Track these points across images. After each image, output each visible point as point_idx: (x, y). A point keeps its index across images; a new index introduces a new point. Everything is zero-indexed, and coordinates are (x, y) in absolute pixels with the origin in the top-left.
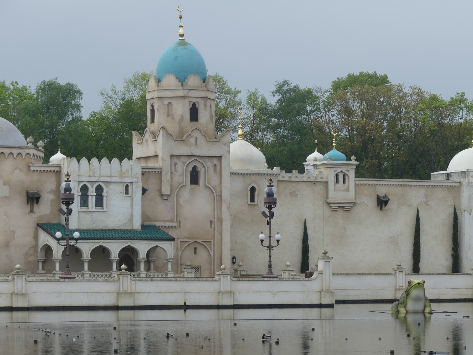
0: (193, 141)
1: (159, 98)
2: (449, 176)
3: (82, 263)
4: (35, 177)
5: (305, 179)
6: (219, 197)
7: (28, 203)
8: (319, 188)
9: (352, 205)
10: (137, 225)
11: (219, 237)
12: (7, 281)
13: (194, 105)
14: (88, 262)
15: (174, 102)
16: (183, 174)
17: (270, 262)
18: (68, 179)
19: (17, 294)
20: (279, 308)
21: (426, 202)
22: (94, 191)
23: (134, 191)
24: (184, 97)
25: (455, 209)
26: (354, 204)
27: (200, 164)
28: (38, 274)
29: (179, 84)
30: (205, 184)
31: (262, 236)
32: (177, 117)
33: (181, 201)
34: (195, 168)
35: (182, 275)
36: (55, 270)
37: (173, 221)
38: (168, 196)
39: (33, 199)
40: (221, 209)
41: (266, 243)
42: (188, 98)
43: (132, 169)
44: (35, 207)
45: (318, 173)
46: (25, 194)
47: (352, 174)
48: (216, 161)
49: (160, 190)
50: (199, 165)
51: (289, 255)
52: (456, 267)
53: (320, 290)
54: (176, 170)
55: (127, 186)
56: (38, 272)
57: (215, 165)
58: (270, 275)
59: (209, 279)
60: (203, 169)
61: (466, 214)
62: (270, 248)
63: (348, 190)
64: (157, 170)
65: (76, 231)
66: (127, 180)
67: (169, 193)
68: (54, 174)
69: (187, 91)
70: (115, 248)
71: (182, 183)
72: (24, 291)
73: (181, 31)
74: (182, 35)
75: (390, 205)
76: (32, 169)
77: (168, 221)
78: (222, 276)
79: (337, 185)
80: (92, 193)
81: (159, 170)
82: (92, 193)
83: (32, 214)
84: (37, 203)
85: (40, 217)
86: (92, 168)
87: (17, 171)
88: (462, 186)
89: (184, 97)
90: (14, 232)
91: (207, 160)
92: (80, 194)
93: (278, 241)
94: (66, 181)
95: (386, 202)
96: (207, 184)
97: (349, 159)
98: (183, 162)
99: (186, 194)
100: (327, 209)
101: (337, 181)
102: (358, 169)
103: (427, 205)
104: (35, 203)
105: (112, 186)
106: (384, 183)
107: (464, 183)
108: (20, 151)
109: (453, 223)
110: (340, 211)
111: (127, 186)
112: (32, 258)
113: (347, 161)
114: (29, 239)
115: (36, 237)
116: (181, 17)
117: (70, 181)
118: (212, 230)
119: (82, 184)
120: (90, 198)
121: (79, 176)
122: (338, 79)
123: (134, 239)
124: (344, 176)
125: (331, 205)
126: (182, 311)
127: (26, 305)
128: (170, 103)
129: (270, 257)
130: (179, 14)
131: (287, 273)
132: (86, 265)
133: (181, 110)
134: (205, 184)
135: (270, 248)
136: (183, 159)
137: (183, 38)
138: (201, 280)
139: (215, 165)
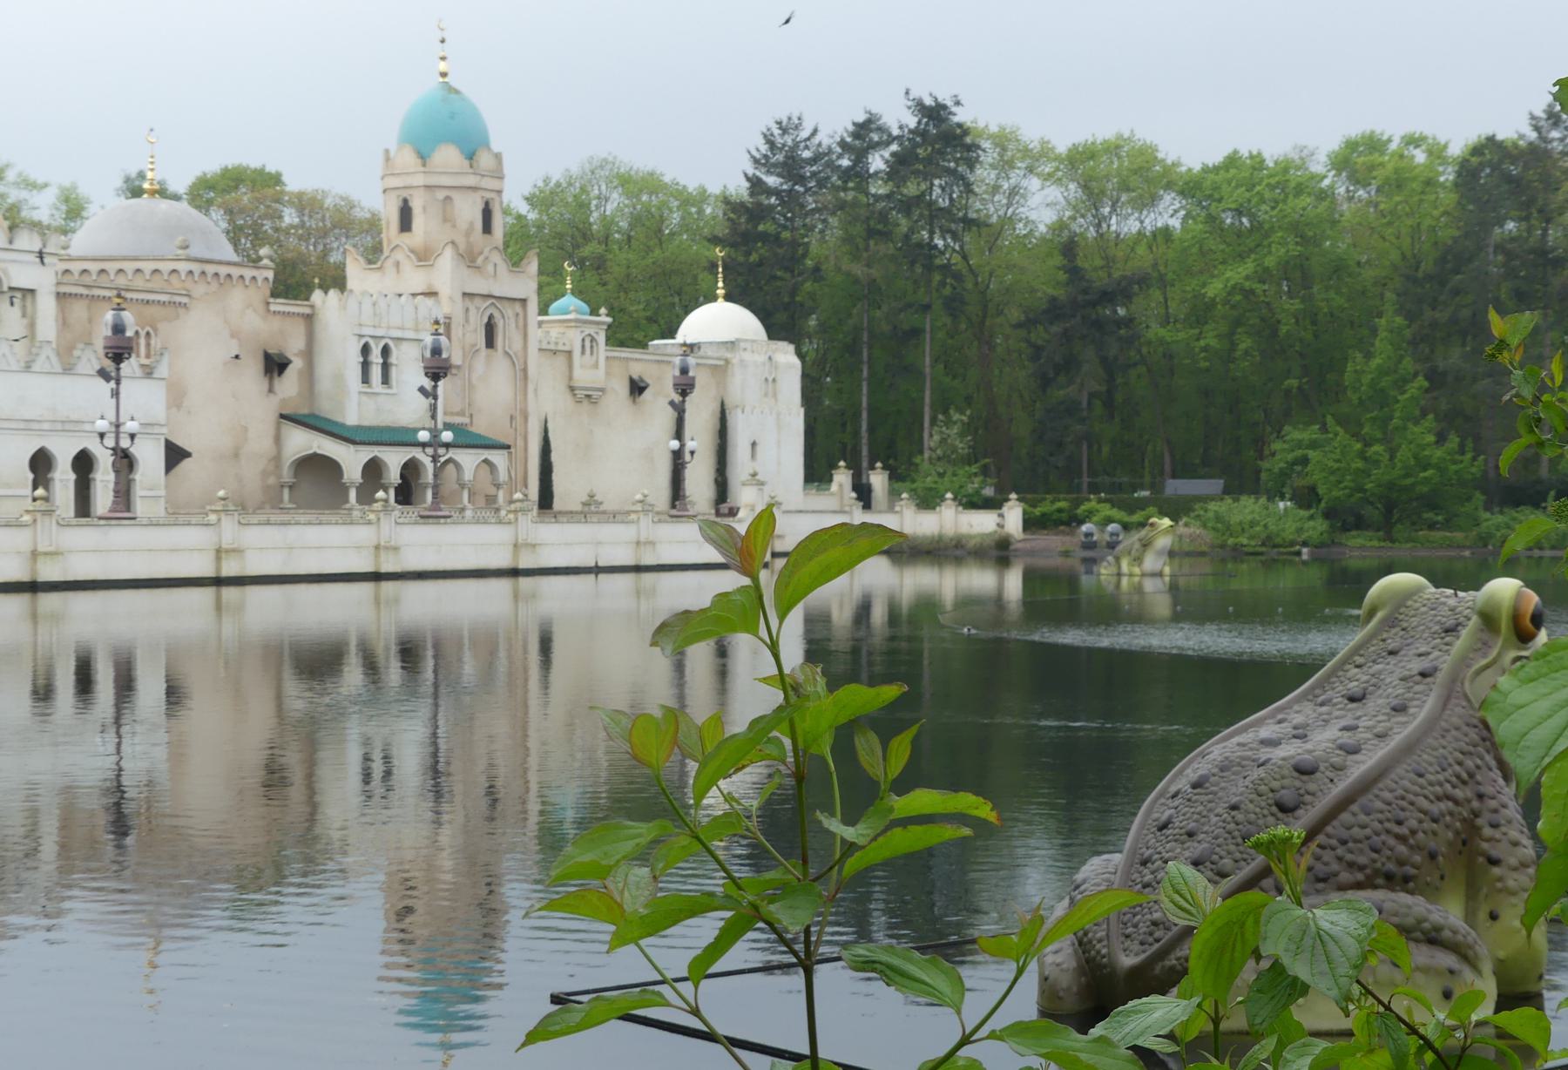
0: (490, 268)
1: (427, 187)
3: (343, 490)
4: (276, 323)
8: (561, 361)
12: (369, 523)
13: (405, 201)
15: (455, 195)
19: (386, 548)
20: (93, 582)
24: (474, 189)
25: (723, 404)
26: (602, 390)
29: (467, 163)
32: (463, 225)
33: (474, 381)
34: (491, 317)
39: (275, 365)
40: (525, 394)
44: (276, 381)
47: (601, 338)
48: (518, 307)
50: (497, 315)
54: (467, 321)
63: (596, 366)
70: (394, 460)
73: (442, 66)
74: (444, 75)
75: (647, 394)
76: (272, 308)
77: (458, 414)
80: (376, 358)
82: (376, 358)
85: (283, 401)
89: (474, 189)
90: (246, 429)
91: (506, 304)
93: (692, 453)
97: (594, 312)
99: (479, 365)
100: (568, 396)
101: (583, 352)
105: (405, 346)
107: (735, 361)
110: (586, 402)
112: (272, 480)
115: (278, 439)
116: (443, 41)
119: (363, 341)
126: (592, 576)
128: (448, 198)
132: (353, 494)
133: (468, 211)
136: (478, 301)
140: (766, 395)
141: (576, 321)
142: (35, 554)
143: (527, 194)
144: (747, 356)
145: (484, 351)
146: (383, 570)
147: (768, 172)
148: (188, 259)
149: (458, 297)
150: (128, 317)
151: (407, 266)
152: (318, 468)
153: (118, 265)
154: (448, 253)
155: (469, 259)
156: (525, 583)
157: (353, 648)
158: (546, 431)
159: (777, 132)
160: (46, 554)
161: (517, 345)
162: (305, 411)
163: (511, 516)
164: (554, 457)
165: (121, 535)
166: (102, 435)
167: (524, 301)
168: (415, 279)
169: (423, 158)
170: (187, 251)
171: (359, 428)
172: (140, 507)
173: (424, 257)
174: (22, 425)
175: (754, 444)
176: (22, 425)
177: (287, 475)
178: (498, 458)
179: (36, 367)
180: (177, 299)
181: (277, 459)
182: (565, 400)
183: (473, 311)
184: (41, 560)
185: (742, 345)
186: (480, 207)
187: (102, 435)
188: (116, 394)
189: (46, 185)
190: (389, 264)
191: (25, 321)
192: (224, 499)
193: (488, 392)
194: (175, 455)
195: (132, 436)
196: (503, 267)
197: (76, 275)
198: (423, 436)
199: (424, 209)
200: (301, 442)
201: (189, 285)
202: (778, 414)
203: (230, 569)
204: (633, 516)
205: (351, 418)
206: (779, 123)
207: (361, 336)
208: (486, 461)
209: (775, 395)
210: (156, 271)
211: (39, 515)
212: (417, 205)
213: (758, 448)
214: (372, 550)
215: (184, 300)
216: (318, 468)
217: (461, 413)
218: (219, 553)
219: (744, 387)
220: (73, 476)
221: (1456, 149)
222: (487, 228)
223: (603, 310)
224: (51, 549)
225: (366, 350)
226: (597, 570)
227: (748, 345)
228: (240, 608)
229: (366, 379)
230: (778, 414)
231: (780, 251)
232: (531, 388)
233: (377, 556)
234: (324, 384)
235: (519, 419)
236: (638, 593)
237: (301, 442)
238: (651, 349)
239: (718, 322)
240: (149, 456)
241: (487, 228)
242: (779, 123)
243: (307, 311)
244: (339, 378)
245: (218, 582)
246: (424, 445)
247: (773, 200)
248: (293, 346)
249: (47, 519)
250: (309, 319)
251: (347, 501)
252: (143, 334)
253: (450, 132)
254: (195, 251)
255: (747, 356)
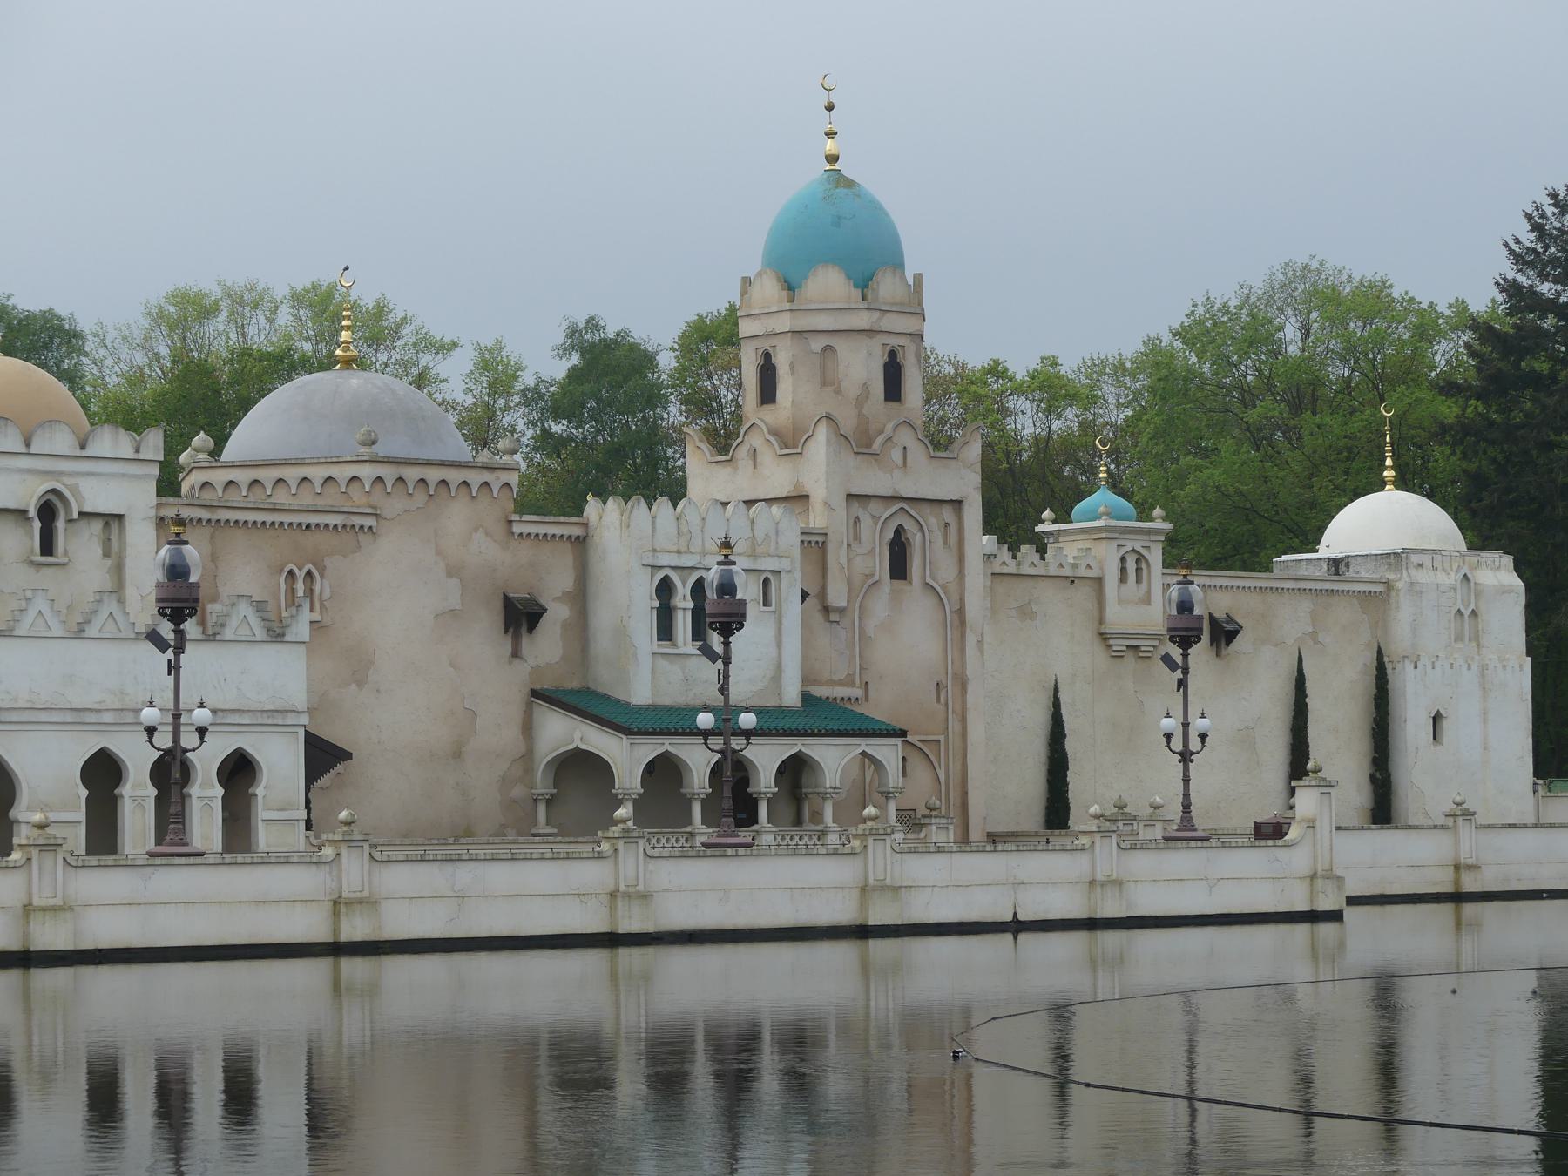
0: (896, 455)
2: (1342, 567)
3: (686, 803)
5: (1053, 571)
6: (956, 617)
7: (506, 632)
8: (1083, 593)
9: (1156, 643)
10: (791, 696)
11: (958, 728)
12: (600, 857)
13: (767, 356)
14: (703, 801)
15: (840, 344)
16: (873, 550)
17: (1186, 795)
18: (726, 556)
19: (628, 896)
20: (553, 947)
21: (1313, 635)
22: (688, 597)
23: (784, 595)
25: (1380, 652)
27: (913, 522)
28: (538, 835)
29: (857, 293)
30: (924, 577)
31: (1168, 724)
32: (851, 388)
33: (871, 625)
34: (899, 531)
35: (922, 835)
36: (690, 823)
37: (853, 684)
38: (841, 611)
39: (521, 616)
40: (962, 650)
41: (1177, 744)
42: (880, 336)
43: (777, 532)
44: (525, 640)
45: (1075, 553)
46: (499, 604)
47: (1156, 556)
48: (947, 514)
49: (822, 594)
50: (909, 526)
51: (1007, 780)
52: (1382, 811)
53: (1308, 872)
54: (857, 537)
55: (766, 582)
56: (534, 831)
57: (947, 525)
58: (1186, 833)
59: (440, 852)
60: (919, 535)
61: (1409, 666)
62: (1186, 757)
63: (1147, 600)
64: (814, 538)
65: (747, 710)
66: (768, 564)
67: (844, 604)
68: (568, 545)
69: (877, 315)
71: (873, 575)
72: (641, 887)
73: (830, 146)
74: (832, 159)
75: (1240, 642)
76: (517, 529)
77: (841, 683)
78: (1097, 837)
79: (1124, 587)
81: (820, 539)
83: (517, 662)
84: (531, 629)
86: (684, 529)
87: (480, 535)
88: (1393, 593)
89: (870, 332)
91: (927, 509)
92: (657, 604)
93: (1203, 737)
94: (719, 563)
95: (1231, 636)
96: (928, 580)
97: (1144, 513)
98: (873, 517)
99: (880, 607)
100: (1098, 648)
101: (1123, 578)
102: (1171, 541)
103: (1316, 642)
104: (524, 630)
106: (1224, 582)
107: (1400, 585)
108: (487, 476)
109: (1374, 691)
110: (1130, 658)
111: (766, 582)
112: (518, 791)
113: (1139, 520)
114: (509, 736)
116: (830, 108)
117: (734, 563)
118: (941, 707)
119: (659, 576)
120: (680, 614)
121: (655, 551)
122: (700, 317)
123: (813, 735)
124: (1138, 561)
125: (1111, 642)
126: (1009, 937)
127: (649, 927)
128: (828, 349)
129: (1186, 780)
130: (824, 99)
131: (1159, 826)
132: (697, 810)
133: (861, 366)
134: (924, 577)
135: (1186, 757)
136: (874, 506)
137: (836, 167)
138: (1000, 847)
139: (947, 525)
140: (1459, 638)
141: (1106, 529)
142: (28, 909)
143: (1176, 326)
144: (1423, 577)
145: (887, 583)
146: (344, 937)
147: (1543, 277)
148: (374, 461)
149: (839, 502)
150: (191, 552)
151: (767, 457)
152: (581, 768)
153: (276, 473)
154: (822, 432)
155: (861, 443)
156: (879, 948)
157: (700, 1044)
158: (1056, 704)
159: (1550, 211)
160: (44, 909)
161: (947, 572)
162: (574, 684)
163: (856, 843)
164: (1070, 745)
165: (175, 880)
166: (151, 731)
167: (957, 504)
168: (776, 478)
169: (790, 288)
170: (375, 448)
171: (653, 708)
172: (264, 837)
173: (790, 442)
174: (69, 717)
175: (1437, 718)
176: (69, 717)
177: (542, 784)
178: (888, 752)
179: (92, 631)
180: (357, 521)
181: (528, 757)
182: (1094, 657)
183: (866, 522)
184: (36, 920)
185: (1415, 559)
186: (879, 360)
187: (151, 731)
188: (174, 668)
189: (454, 345)
190: (742, 452)
191: (108, 562)
192: (348, 824)
193: (902, 645)
194: (322, 756)
195: (202, 731)
196: (918, 453)
197: (293, 485)
198: (705, 720)
199: (792, 367)
200: (560, 732)
201: (377, 497)
202: (1483, 669)
203: (355, 929)
204: (1084, 840)
205: (640, 693)
206: (1554, 196)
207: (655, 568)
208: (863, 754)
209: (1476, 637)
210: (255, 482)
211: (35, 853)
212: (782, 361)
213: (1445, 724)
214: (605, 899)
215: (369, 522)
216: (581, 768)
217: (849, 682)
218: (338, 905)
219: (1418, 626)
220: (152, 792)
221: (1357, 276)
222: (893, 388)
223: (1158, 512)
224: (58, 902)
225: (665, 589)
226: (1017, 927)
227: (1426, 560)
228: (372, 991)
229: (665, 631)
230: (1483, 669)
231: (1550, 402)
232: (971, 640)
233: (612, 908)
234: (602, 642)
235: (951, 689)
236: (1093, 963)
237: (560, 732)
238: (1276, 572)
239: (1383, 521)
240: (282, 764)
241: (893, 388)
242: (1554, 196)
243: (577, 531)
244: (621, 633)
245: (335, 949)
246: (706, 734)
247: (1549, 323)
248: (554, 583)
249: (48, 858)
250: (581, 543)
251: (689, 822)
252: (300, 575)
253: (845, 243)
254: (381, 450)
255: (1423, 577)
